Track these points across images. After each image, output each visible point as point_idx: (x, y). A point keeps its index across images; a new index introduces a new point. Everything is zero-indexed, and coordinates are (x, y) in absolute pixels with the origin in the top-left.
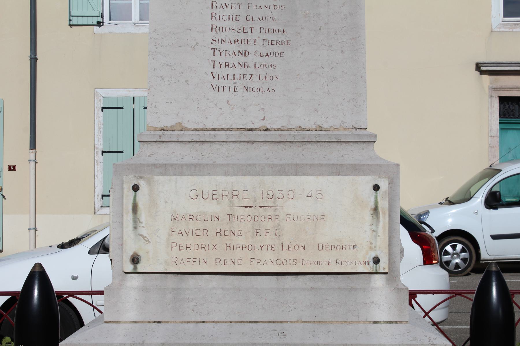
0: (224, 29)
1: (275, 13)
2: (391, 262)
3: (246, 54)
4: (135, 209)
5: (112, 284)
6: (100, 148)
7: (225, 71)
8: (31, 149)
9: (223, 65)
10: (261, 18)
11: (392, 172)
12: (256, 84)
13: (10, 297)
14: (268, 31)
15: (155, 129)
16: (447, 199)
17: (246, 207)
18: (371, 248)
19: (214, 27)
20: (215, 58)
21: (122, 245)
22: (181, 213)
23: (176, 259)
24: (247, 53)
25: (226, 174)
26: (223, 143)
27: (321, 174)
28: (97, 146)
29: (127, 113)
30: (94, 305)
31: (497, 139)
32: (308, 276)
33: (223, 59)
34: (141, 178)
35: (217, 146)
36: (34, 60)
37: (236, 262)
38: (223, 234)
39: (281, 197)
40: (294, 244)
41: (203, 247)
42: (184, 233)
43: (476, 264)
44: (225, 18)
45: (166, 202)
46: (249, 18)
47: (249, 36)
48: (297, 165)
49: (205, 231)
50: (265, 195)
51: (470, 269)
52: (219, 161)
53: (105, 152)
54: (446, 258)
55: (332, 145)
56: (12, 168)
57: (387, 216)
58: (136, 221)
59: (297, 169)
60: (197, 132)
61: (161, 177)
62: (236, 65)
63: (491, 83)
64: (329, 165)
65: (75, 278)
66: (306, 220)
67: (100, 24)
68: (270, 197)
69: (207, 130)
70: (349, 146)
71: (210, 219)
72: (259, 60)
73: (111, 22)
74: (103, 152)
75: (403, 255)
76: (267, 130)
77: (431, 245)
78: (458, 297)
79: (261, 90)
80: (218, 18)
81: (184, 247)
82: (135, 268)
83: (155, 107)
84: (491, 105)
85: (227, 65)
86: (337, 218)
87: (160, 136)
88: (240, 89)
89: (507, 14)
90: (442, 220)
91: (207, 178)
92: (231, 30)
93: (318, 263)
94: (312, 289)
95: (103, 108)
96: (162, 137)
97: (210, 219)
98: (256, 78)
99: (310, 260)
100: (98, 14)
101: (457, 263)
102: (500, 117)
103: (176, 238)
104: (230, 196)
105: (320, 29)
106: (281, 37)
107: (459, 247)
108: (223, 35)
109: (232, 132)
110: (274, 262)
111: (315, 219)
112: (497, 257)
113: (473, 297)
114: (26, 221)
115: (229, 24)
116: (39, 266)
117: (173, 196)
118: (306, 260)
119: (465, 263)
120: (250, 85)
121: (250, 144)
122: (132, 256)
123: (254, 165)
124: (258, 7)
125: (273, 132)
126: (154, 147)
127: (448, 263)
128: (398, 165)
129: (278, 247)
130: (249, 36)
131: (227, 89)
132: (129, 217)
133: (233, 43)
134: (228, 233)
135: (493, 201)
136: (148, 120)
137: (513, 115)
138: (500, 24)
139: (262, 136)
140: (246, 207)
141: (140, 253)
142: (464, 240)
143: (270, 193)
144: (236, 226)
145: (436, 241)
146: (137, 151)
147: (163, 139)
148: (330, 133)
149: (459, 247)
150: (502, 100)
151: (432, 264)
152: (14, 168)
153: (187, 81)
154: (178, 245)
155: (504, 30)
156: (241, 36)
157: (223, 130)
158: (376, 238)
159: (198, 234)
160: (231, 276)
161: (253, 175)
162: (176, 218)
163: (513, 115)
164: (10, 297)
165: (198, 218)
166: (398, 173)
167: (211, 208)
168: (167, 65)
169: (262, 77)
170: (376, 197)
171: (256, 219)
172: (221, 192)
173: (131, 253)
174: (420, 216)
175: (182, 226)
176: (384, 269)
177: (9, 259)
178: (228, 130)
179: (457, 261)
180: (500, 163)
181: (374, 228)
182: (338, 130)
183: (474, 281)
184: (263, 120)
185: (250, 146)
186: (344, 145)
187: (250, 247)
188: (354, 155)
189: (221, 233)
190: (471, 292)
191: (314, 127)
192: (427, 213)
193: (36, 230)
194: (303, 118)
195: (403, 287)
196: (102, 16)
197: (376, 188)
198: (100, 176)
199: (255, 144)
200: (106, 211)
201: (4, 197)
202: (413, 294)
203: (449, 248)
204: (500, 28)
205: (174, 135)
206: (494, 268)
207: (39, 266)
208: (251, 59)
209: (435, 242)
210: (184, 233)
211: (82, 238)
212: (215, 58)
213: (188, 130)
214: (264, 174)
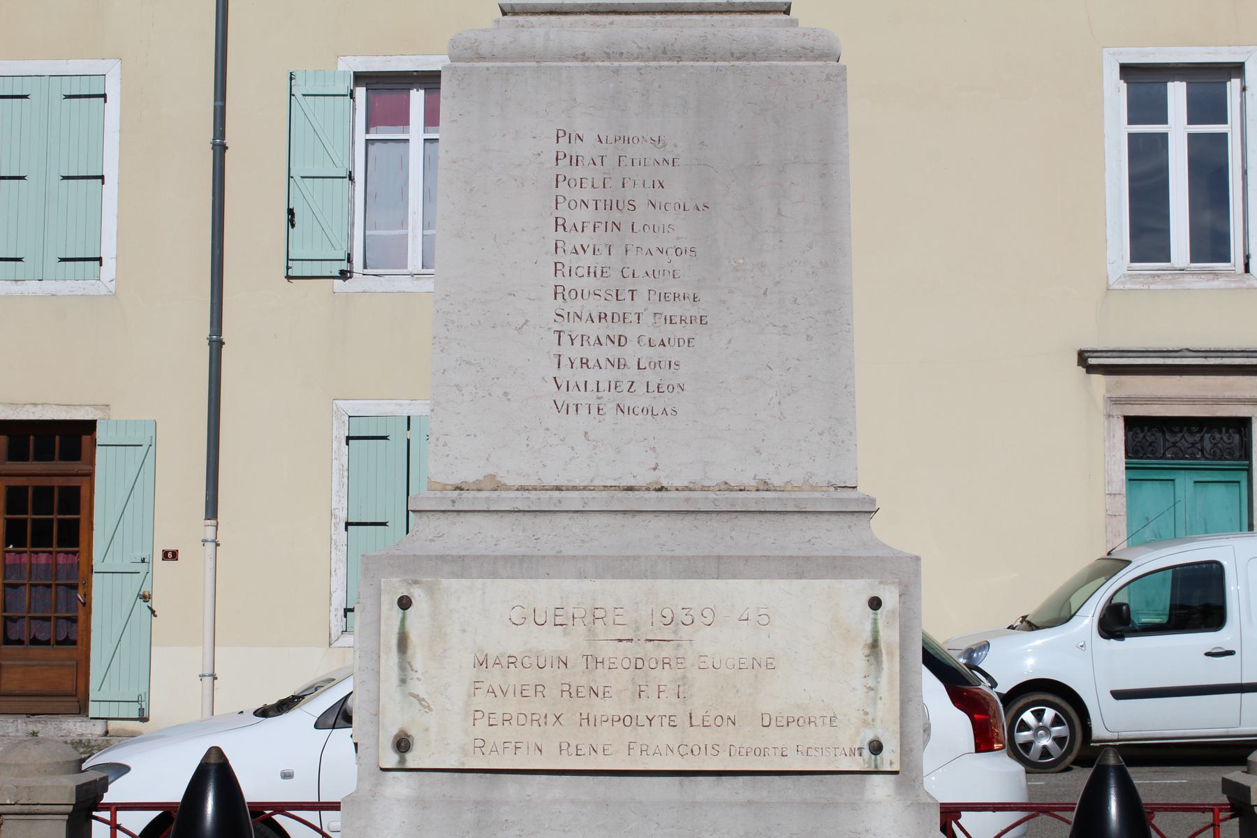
0: (579, 294)
1: (678, 263)
2: (905, 750)
3: (620, 341)
4: (403, 643)
5: (356, 791)
6: (343, 516)
7: (580, 375)
8: (207, 518)
9: (577, 363)
10: (650, 273)
11: (906, 572)
12: (640, 400)
13: (159, 812)
14: (663, 297)
15: (444, 488)
16: (1024, 618)
17: (620, 640)
18: (865, 723)
19: (560, 290)
20: (561, 350)
21: (377, 714)
22: (492, 654)
23: (481, 744)
24: (623, 339)
25: (582, 575)
26: (576, 515)
27: (767, 576)
28: (337, 512)
29: (396, 446)
30: (325, 830)
31: (1121, 501)
32: (741, 779)
33: (576, 352)
34: (416, 582)
35: (564, 520)
36: (216, 346)
37: (600, 750)
38: (574, 694)
39: (688, 620)
40: (713, 714)
41: (534, 719)
42: (498, 692)
43: (1082, 748)
44: (580, 272)
45: (464, 631)
46: (628, 273)
47: (627, 306)
48: (719, 558)
49: (539, 688)
50: (658, 616)
51: (1071, 758)
52: (568, 550)
53: (352, 524)
54: (1023, 736)
55: (788, 518)
56: (170, 555)
57: (897, 659)
58: (404, 666)
59: (721, 566)
60: (526, 494)
61: (454, 581)
62: (603, 362)
63: (1108, 390)
64: (783, 557)
65: (287, 775)
66: (737, 666)
67: (345, 275)
68: (668, 620)
69: (544, 489)
70: (823, 522)
71: (549, 665)
72: (646, 353)
73: (366, 271)
74: (348, 524)
75: (929, 735)
76: (661, 489)
77: (991, 712)
78: (1043, 817)
79: (649, 411)
80: (567, 273)
81: (497, 719)
82: (402, 760)
83: (445, 445)
84: (1109, 433)
85: (584, 363)
86: (798, 664)
87: (453, 502)
88: (610, 409)
89: (1136, 256)
90: (1012, 663)
91: (543, 583)
92: (592, 296)
93: (761, 753)
94: (749, 803)
95: (349, 438)
96: (459, 503)
97: (549, 665)
98: (640, 388)
99: (746, 745)
100: (343, 256)
101: (1045, 747)
102: (1127, 456)
103: (483, 701)
104: (589, 619)
105: (765, 293)
106: (688, 309)
107: (1049, 714)
108: (576, 306)
109: (594, 494)
110: (676, 750)
111: (756, 665)
112: (1124, 735)
113: (1071, 816)
114: (196, 659)
115: (589, 283)
116: (216, 752)
117: (477, 618)
118: (737, 745)
119: (1061, 746)
120: (628, 401)
121: (629, 516)
122: (396, 736)
123: (636, 558)
124: (645, 250)
125: (673, 494)
126: (442, 523)
127: (1027, 746)
128: (918, 559)
129: (682, 720)
130: (627, 306)
131: (583, 410)
132: (390, 659)
133: (596, 320)
134: (584, 692)
135: (1116, 623)
136: (433, 467)
137: (1153, 452)
138: (1125, 276)
139: (651, 500)
140: (620, 640)
141: (412, 732)
142: (1058, 700)
143: (667, 612)
144: (600, 678)
145: (1001, 705)
146: (412, 525)
147: (458, 507)
148: (786, 495)
149: (1049, 714)
150: (1132, 423)
151: (992, 750)
152: (175, 555)
153: (506, 394)
154: (486, 715)
155: (1132, 287)
156: (611, 307)
157: (575, 488)
158: (875, 703)
159: (525, 693)
160: (591, 778)
161: (633, 578)
162: (482, 663)
163: (1153, 452)
164: (159, 812)
165: (526, 661)
166: (917, 573)
167: (551, 642)
168: (468, 362)
169: (653, 387)
170: (875, 621)
171: (640, 664)
172: (571, 612)
173: (395, 731)
174: (969, 653)
175: (494, 677)
176: (891, 763)
177: (161, 737)
178: (585, 488)
179: (1046, 742)
180: (1239, 432)
181: (871, 683)
182: (801, 489)
183: (1075, 783)
184: (655, 469)
185: (628, 519)
186: (811, 518)
187: (628, 719)
188: (831, 538)
189: (571, 692)
190: (1068, 808)
191: (753, 483)
192: (986, 646)
193: (215, 678)
194: (733, 466)
195: (929, 800)
196: (349, 260)
197: (875, 603)
198: (342, 571)
199: (639, 518)
200: (348, 640)
201: (153, 612)
202: (950, 813)
203: (1028, 717)
204: (1123, 283)
205: (480, 499)
206: (1112, 760)
207: (216, 752)
208: (631, 352)
209: (997, 706)
210: (498, 692)
211: (303, 697)
212: (561, 350)
213: (509, 489)
214: (655, 576)
